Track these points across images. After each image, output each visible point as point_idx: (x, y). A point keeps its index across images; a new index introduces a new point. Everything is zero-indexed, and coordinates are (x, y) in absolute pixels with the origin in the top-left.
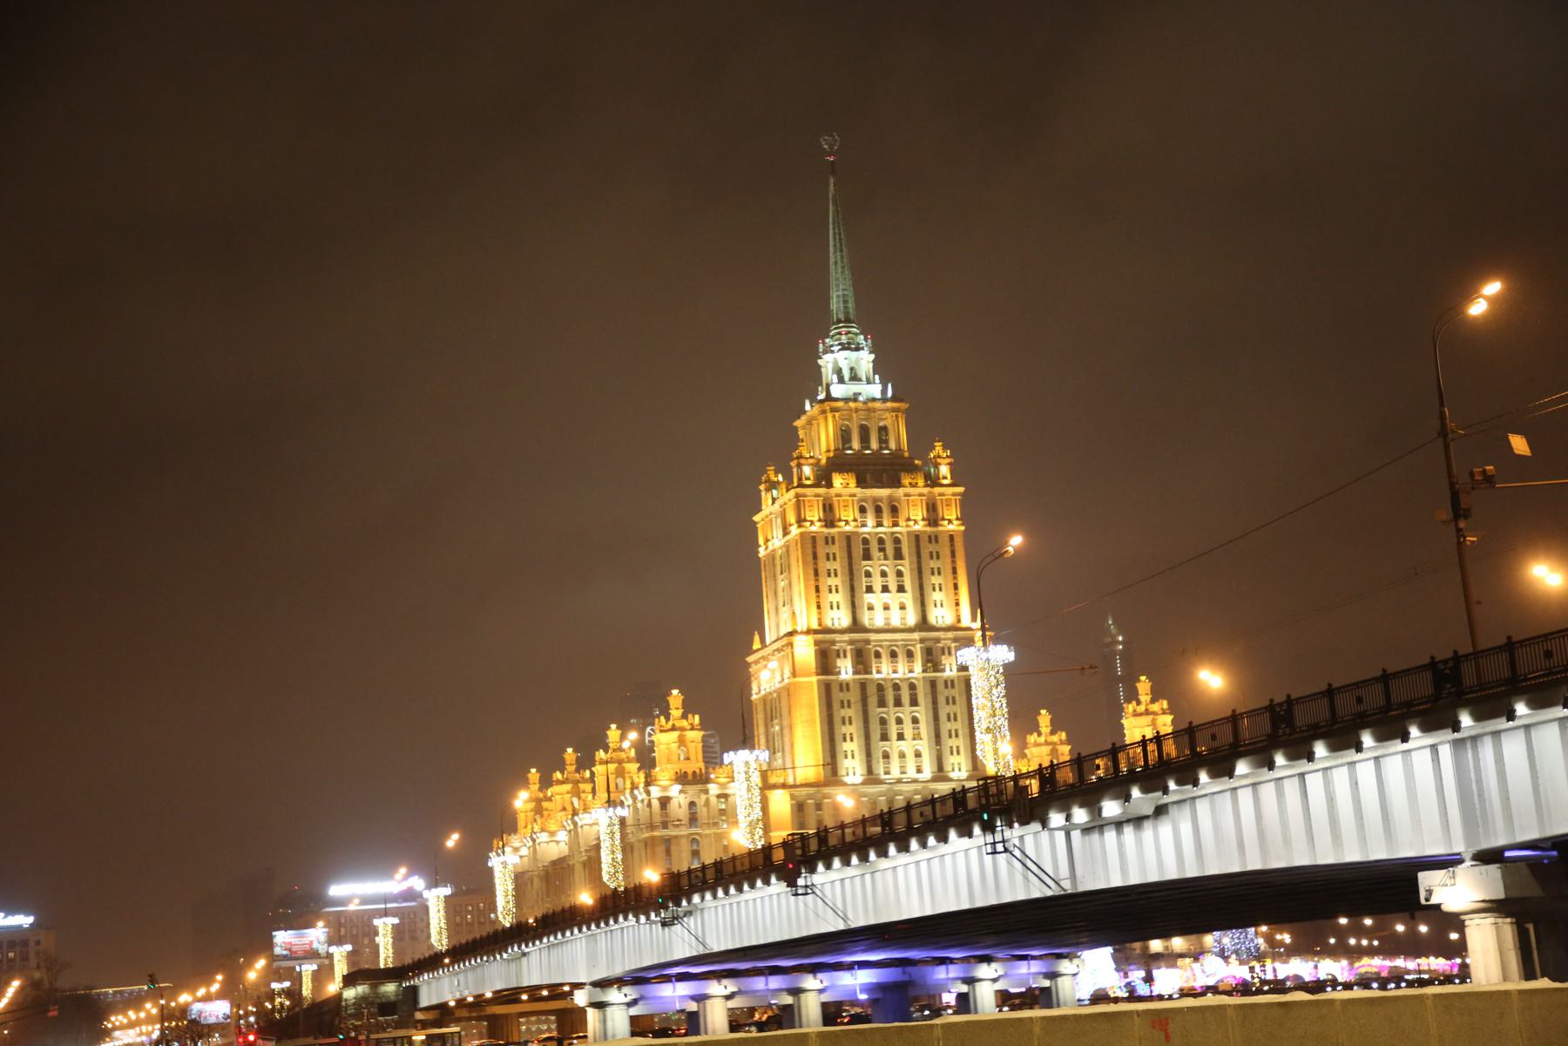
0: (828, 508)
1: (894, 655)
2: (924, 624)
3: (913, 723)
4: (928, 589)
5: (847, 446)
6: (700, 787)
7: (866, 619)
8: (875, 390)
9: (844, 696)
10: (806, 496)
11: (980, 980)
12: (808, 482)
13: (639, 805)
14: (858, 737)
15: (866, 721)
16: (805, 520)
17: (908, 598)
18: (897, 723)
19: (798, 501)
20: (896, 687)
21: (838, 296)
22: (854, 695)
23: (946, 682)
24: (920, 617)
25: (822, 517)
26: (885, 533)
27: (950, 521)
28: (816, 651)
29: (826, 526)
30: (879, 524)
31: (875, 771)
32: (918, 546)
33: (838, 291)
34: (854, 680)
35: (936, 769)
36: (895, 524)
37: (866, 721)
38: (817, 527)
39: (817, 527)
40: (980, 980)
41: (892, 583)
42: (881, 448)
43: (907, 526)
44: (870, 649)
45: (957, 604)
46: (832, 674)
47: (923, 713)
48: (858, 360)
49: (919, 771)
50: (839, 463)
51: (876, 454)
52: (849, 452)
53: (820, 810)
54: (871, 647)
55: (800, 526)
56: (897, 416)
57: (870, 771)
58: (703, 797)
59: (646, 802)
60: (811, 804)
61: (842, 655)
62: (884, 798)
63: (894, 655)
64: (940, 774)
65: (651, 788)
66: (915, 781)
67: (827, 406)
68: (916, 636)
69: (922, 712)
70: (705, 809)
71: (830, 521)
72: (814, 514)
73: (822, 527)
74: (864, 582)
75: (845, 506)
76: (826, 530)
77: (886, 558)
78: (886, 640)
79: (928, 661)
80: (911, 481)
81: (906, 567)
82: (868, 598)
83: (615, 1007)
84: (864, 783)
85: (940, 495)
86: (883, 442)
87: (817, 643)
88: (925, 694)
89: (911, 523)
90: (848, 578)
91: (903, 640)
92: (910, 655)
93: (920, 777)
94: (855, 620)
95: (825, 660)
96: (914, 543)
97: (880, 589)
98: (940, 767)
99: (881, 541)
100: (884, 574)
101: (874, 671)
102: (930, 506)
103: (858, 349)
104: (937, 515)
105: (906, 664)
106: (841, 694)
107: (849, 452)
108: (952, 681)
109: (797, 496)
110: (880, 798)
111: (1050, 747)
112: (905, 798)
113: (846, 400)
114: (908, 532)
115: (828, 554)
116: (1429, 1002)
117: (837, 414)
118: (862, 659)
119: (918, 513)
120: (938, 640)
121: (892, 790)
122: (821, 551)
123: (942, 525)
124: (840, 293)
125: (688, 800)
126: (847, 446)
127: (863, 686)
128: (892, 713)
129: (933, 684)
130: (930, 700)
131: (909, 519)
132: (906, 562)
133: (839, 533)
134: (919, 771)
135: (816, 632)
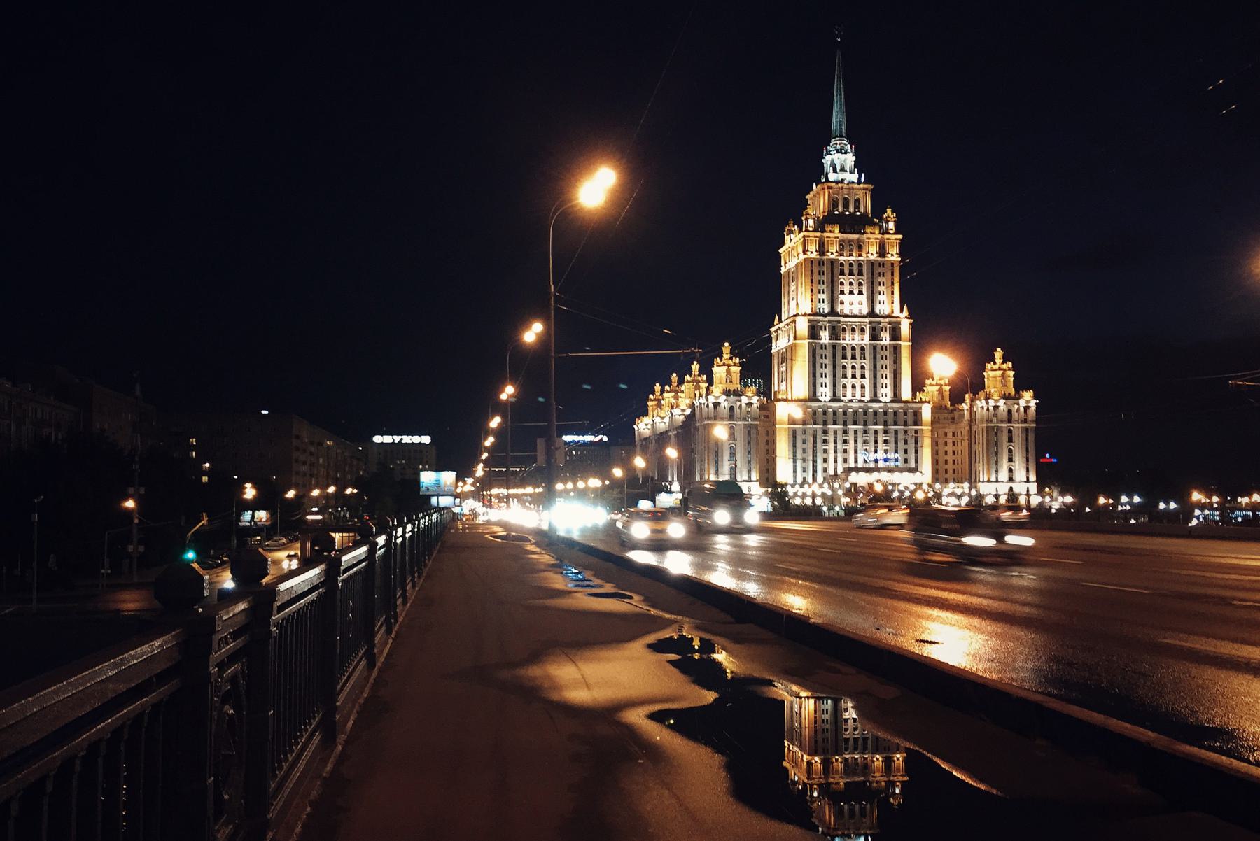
1: (853, 330)
2: (872, 313)
9: (823, 352)
15: (835, 367)
17: (864, 298)
19: (804, 241)
22: (829, 353)
26: (854, 261)
28: (809, 326)
29: (880, 256)
30: (851, 255)
34: (890, 344)
36: (860, 255)
37: (835, 367)
38: (814, 255)
45: (893, 303)
49: (863, 396)
51: (853, 214)
55: (804, 254)
56: (866, 193)
57: (835, 394)
58: (738, 403)
63: (853, 330)
64: (875, 399)
67: (825, 185)
68: (867, 320)
70: (739, 411)
86: (857, 207)
87: (809, 321)
92: (863, 330)
98: (875, 394)
106: (882, 352)
108: (886, 347)
109: (804, 237)
113: (837, 182)
117: (831, 190)
118: (834, 334)
120: (880, 323)
127: (834, 347)
129: (875, 347)
131: (868, 253)
134: (863, 396)
135: (809, 315)
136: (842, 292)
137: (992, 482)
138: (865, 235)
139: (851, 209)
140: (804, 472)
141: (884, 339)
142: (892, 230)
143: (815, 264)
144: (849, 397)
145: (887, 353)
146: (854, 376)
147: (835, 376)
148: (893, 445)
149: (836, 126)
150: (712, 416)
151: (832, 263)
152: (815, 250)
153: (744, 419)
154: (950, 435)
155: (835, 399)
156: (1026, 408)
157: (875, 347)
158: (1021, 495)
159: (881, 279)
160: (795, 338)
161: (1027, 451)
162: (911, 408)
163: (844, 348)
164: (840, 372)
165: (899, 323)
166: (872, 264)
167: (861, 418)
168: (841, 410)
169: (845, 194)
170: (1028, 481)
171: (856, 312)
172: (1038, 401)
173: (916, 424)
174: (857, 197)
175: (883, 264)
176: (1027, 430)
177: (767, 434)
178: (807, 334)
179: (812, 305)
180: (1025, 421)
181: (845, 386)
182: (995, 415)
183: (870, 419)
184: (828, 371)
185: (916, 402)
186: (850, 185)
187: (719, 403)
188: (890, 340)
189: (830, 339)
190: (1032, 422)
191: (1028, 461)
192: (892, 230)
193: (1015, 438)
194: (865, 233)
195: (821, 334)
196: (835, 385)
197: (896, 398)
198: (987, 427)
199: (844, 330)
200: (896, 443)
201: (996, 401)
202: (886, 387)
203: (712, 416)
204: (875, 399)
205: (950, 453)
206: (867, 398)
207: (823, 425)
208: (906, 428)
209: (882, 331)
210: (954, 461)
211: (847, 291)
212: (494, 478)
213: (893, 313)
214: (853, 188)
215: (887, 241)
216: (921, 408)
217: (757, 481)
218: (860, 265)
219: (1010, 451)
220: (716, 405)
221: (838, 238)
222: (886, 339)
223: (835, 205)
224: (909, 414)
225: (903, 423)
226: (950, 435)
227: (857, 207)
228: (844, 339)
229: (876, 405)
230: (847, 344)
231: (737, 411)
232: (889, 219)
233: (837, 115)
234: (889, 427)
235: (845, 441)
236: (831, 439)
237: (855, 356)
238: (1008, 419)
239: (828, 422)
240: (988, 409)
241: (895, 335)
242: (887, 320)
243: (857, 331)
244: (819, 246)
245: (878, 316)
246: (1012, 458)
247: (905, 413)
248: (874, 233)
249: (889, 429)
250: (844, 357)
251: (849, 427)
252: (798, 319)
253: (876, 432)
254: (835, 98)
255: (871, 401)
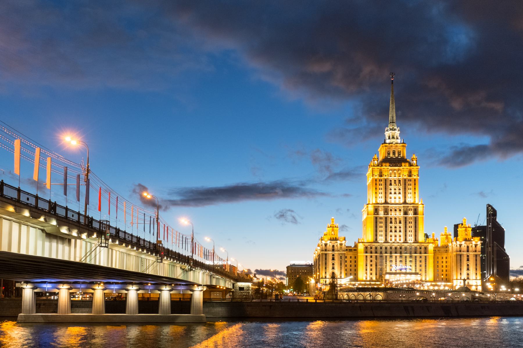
0: (410, 172)
1: (396, 210)
2: (405, 203)
3: (395, 228)
4: (407, 193)
5: (389, 156)
6: (335, 241)
7: (389, 201)
8: (399, 141)
9: (381, 220)
10: (375, 169)
11: (163, 290)
12: (415, 165)
13: (453, 246)
14: (384, 231)
15: (386, 227)
16: (374, 175)
17: (401, 196)
18: (390, 228)
19: (373, 170)
20: (395, 219)
21: (391, 116)
22: (383, 221)
23: (380, 218)
24: (404, 201)
25: (379, 174)
26: (396, 179)
27: (415, 176)
28: (374, 209)
29: (380, 176)
30: (395, 176)
31: (407, 240)
32: (405, 182)
33: (391, 115)
34: (413, 217)
35: (404, 240)
36: (400, 176)
37: (386, 227)
38: (377, 177)
39: (377, 177)
40: (163, 290)
41: (397, 192)
42: (398, 156)
43: (402, 177)
44: (389, 209)
45: (415, 198)
46: (417, 215)
47: (402, 226)
48: (394, 133)
49: (400, 240)
50: (386, 160)
51: (397, 158)
52: (400, 157)
53: (421, 249)
54: (389, 208)
55: (373, 176)
56: (403, 148)
57: (386, 239)
58: (336, 244)
59: (456, 245)
60: (413, 248)
61: (410, 210)
62: (389, 247)
63: (396, 210)
64: (406, 241)
65: (457, 242)
66: (398, 243)
67: (384, 145)
68: (402, 205)
69: (402, 225)
70: (336, 247)
71: (410, 175)
72: (377, 173)
73: (379, 177)
74: (389, 191)
75: (385, 171)
76: (380, 178)
77: (396, 185)
78: (393, 207)
79: (376, 212)
80: (405, 165)
81: (401, 188)
82: (390, 195)
83: (196, 291)
84: (414, 243)
85: (413, 168)
86: (399, 154)
87: (374, 207)
88: (403, 221)
89: (404, 176)
90: (385, 190)
91: (398, 207)
92: (400, 210)
93: (400, 242)
94: (386, 201)
95: (376, 211)
96: (404, 181)
97: (398, 193)
98: (406, 240)
99: (395, 181)
100: (395, 189)
101: (389, 214)
102: (410, 171)
103: (395, 130)
104: (411, 174)
105: (399, 213)
106: (380, 220)
107: (400, 157)
108: (382, 218)
109: (373, 169)
110: (388, 247)
111: (446, 236)
112: (405, 247)
113: (389, 144)
114: (403, 178)
115: (380, 184)
116: (21, 298)
117: (386, 147)
118: (386, 212)
119: (406, 173)
120: (408, 207)
121: (421, 245)
122: (378, 183)
123: (412, 177)
124: (392, 115)
125: (467, 245)
126: (389, 156)
127: (386, 218)
128: (398, 225)
129: (406, 218)
130: (404, 222)
131: (403, 175)
132: (401, 186)
133: (383, 178)
134: (400, 240)
135: (374, 204)
136: (391, 193)
137: (458, 279)
138: (401, 167)
139: (397, 155)
140: (371, 275)
141: (410, 214)
142: (415, 164)
143: (378, 181)
144: (393, 240)
145: (412, 221)
146: (396, 231)
147: (386, 231)
148: (414, 263)
149: (391, 118)
150: (324, 249)
151: (386, 180)
152: (407, 174)
153: (339, 251)
154: (444, 258)
155: (386, 242)
156: (476, 246)
157: (406, 218)
158: (472, 285)
159: (410, 187)
160: (368, 215)
161: (476, 265)
162: (423, 246)
163: (391, 219)
164: (389, 229)
165: (418, 207)
166: (405, 180)
167: (399, 250)
168: (389, 247)
169: (393, 149)
170: (476, 279)
171: (397, 202)
172: (482, 242)
173: (425, 253)
174: (399, 150)
175: (411, 180)
176: (476, 256)
177: (355, 258)
178: (373, 213)
179: (376, 199)
180: (476, 251)
181: (391, 236)
182: (341, 248)
183: (403, 250)
184: (383, 229)
185: (426, 243)
186: (396, 145)
187: (462, 245)
188: (413, 215)
189: (384, 215)
190: (479, 251)
191: (476, 269)
192: (415, 164)
193: (470, 259)
194: (401, 166)
195: (409, 212)
196: (386, 235)
197: (416, 241)
198: (456, 254)
199: (391, 210)
200: (416, 262)
201: (461, 242)
202: (411, 236)
203: (324, 249)
204: (406, 241)
205: (444, 266)
206: (402, 241)
207: (410, 254)
208: (421, 255)
209: (409, 210)
210: (446, 270)
211: (393, 193)
212: (277, 279)
213: (415, 202)
214: (397, 146)
215: (383, 169)
216: (428, 246)
217: (480, 280)
218: (400, 181)
219: (468, 265)
220: (326, 245)
221: (388, 169)
222: (411, 214)
223: (389, 154)
224: (422, 249)
225: (409, 253)
226: (444, 258)
227: (399, 154)
228: (391, 215)
229: (406, 244)
230: (397, 217)
231: (336, 248)
232: (413, 159)
233: (391, 113)
234: (412, 254)
235: (391, 261)
236: (404, 260)
237: (401, 222)
238: (467, 250)
239: (412, 252)
240: (457, 246)
241: (416, 212)
242: (412, 205)
243: (397, 210)
244: (409, 173)
245: (407, 204)
246: (469, 269)
247: (420, 248)
248: (406, 166)
249: (413, 255)
250: (391, 223)
251: (403, 254)
252: (369, 205)
253: (406, 257)
254: (390, 105)
255: (404, 243)
